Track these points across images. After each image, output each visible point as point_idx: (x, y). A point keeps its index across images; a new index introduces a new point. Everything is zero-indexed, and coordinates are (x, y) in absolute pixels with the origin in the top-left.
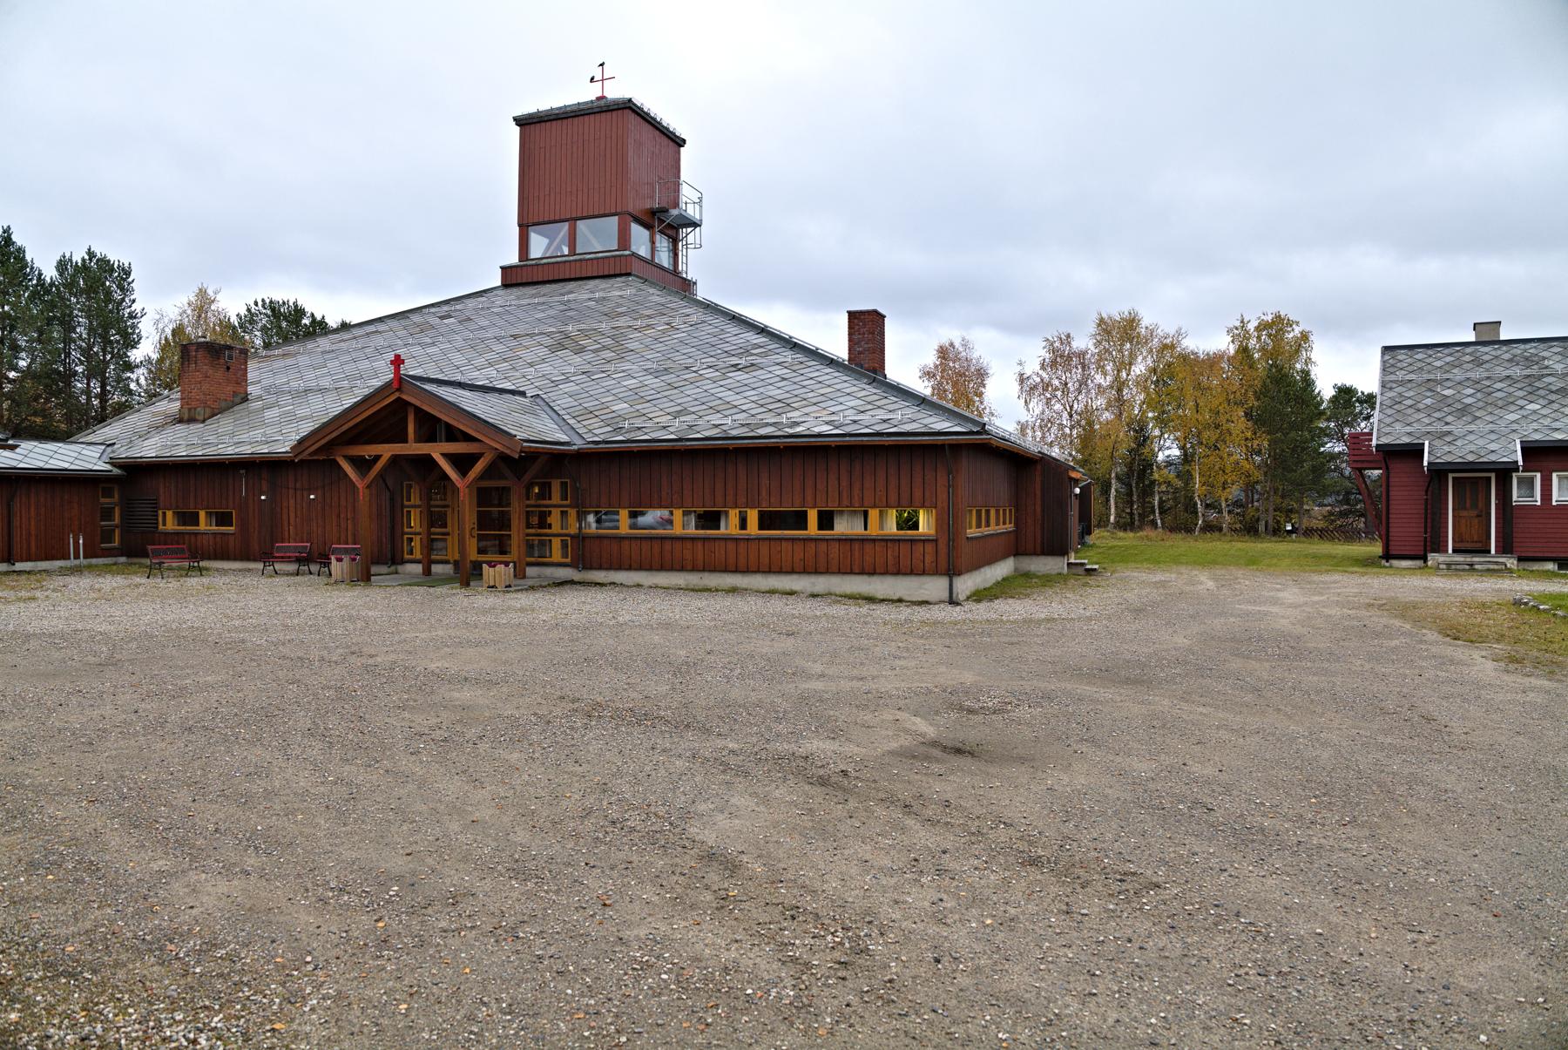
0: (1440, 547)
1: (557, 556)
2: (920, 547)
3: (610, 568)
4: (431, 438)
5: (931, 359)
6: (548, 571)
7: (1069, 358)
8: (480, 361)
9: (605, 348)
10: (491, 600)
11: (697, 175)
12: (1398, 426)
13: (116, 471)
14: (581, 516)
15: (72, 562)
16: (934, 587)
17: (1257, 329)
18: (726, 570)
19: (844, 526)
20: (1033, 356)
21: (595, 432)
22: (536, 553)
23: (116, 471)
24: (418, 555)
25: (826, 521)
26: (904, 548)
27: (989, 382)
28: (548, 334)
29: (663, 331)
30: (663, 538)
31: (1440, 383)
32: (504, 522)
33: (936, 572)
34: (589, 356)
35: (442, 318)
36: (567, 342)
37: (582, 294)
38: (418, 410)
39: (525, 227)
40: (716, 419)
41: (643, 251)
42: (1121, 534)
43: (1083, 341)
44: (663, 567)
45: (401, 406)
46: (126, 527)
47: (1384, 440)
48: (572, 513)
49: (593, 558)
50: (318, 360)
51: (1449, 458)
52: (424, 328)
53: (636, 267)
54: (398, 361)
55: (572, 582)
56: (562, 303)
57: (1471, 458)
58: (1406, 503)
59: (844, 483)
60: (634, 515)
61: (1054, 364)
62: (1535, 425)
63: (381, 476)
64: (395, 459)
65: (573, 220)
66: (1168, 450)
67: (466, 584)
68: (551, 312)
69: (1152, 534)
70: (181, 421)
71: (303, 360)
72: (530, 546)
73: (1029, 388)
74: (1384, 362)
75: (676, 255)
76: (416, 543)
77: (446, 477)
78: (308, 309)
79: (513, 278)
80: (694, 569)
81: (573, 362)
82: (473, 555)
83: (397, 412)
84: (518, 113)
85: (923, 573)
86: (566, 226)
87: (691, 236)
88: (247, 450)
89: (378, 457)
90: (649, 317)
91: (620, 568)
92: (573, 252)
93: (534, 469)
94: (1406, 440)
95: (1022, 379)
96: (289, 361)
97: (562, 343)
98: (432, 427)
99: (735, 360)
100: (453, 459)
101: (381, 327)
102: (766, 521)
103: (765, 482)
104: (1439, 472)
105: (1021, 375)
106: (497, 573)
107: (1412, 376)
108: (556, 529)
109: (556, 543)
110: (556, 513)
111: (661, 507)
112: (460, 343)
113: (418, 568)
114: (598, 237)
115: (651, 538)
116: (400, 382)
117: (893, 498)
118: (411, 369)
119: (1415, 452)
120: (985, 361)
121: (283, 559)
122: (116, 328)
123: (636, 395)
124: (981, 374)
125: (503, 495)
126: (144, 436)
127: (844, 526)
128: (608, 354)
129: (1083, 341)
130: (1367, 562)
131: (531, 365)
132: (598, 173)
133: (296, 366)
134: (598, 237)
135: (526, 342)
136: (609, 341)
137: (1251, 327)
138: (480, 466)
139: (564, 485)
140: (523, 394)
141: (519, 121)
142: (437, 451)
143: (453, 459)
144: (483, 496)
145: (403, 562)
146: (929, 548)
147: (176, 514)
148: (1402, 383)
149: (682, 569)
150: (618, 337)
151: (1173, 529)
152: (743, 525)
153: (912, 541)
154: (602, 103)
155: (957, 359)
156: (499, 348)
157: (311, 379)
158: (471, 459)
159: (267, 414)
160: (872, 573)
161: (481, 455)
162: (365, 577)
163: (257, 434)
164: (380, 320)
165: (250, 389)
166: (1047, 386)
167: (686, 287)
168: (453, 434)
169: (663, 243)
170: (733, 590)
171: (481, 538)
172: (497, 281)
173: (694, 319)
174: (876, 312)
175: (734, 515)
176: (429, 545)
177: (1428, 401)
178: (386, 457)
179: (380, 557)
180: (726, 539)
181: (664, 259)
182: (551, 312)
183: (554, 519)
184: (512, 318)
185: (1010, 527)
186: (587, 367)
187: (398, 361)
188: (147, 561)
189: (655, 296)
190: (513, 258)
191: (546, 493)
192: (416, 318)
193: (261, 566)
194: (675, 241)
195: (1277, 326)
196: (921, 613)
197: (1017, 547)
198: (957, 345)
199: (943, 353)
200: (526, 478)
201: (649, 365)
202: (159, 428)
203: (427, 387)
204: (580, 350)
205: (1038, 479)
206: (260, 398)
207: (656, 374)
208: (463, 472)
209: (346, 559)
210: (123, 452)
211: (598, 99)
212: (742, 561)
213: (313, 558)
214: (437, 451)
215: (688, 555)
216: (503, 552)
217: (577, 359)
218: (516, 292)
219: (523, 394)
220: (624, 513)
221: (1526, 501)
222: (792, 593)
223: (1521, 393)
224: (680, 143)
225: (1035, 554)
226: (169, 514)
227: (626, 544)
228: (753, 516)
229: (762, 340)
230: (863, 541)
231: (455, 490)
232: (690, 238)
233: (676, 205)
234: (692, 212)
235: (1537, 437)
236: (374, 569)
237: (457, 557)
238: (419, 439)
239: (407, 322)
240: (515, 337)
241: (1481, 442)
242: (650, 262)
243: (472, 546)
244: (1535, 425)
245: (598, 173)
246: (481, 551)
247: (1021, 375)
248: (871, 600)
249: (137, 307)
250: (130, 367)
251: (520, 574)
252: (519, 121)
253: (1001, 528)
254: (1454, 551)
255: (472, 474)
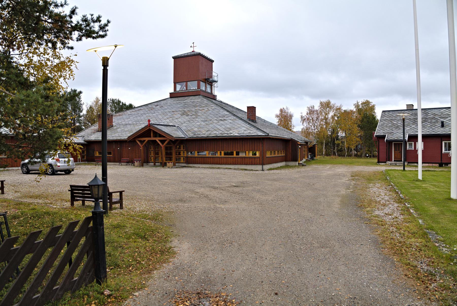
0: (390, 159)
1: (182, 161)
2: (256, 159)
3: (193, 163)
4: (156, 137)
5: (278, 113)
6: (180, 164)
7: (314, 112)
8: (165, 118)
9: (193, 115)
10: (169, 169)
11: (217, 70)
12: (381, 131)
13: (86, 143)
14: (187, 152)
15: (78, 163)
16: (259, 167)
17: (361, 104)
18: (217, 164)
19: (241, 155)
20: (305, 112)
21: (190, 135)
22: (178, 160)
23: (86, 143)
24: (152, 161)
25: (238, 154)
26: (253, 159)
27: (293, 118)
28: (181, 111)
29: (206, 111)
30: (204, 157)
31: (394, 120)
32: (171, 154)
33: (259, 164)
34: (190, 117)
35: (156, 106)
36: (185, 113)
37: (189, 100)
38: (153, 131)
39: (175, 83)
40: (215, 132)
41: (203, 88)
42: (326, 157)
43: (317, 107)
44: (204, 163)
45: (150, 130)
46: (87, 155)
47: (377, 134)
48: (185, 152)
49: (190, 161)
50: (128, 117)
51: (391, 139)
52: (152, 109)
53: (202, 93)
54: (149, 121)
55: (185, 167)
56: (184, 103)
57: (396, 139)
58: (383, 148)
59: (241, 146)
60: (198, 152)
61: (310, 113)
62: (413, 131)
63: (145, 145)
64: (148, 141)
65: (187, 82)
66: (341, 134)
67: (163, 167)
68: (182, 105)
69: (334, 157)
70: (98, 131)
71: (124, 116)
72: (177, 160)
73: (303, 119)
74: (382, 115)
75: (212, 89)
76: (152, 158)
77: (159, 144)
78: (122, 101)
79: (172, 96)
80: (211, 164)
81: (186, 118)
82: (165, 161)
83: (149, 131)
84: (173, 56)
85: (257, 164)
86: (185, 83)
87: (215, 84)
88: (115, 138)
89: (145, 141)
90: (204, 107)
91: (195, 163)
92: (187, 89)
93: (178, 142)
94: (382, 134)
95: (302, 117)
96: (121, 117)
97: (184, 113)
98: (157, 134)
99: (221, 118)
100: (160, 141)
101: (142, 108)
102: (225, 154)
103: (256, 145)
104: (390, 142)
105: (302, 116)
106: (170, 164)
107: (388, 118)
108: (182, 155)
109: (182, 158)
110: (182, 152)
111: (206, 151)
112: (160, 113)
113: (153, 164)
114: (193, 86)
115: (202, 157)
116: (150, 125)
117: (251, 149)
118: (152, 122)
119: (384, 137)
120: (292, 113)
121: (124, 162)
122: (77, 107)
123: (199, 127)
124: (291, 116)
125: (171, 148)
126: (91, 135)
127: (241, 155)
128: (194, 116)
129: (317, 107)
130: (373, 164)
131: (177, 119)
132: (193, 71)
133: (123, 118)
134: (193, 86)
135: (176, 113)
136: (194, 113)
137: (360, 103)
138: (166, 142)
139: (184, 146)
140: (175, 126)
141: (173, 58)
142: (157, 139)
143: (160, 141)
144: (166, 148)
145: (149, 162)
146: (258, 159)
147: (99, 152)
148: (385, 120)
149: (208, 164)
150: (196, 112)
151: (339, 155)
152: (221, 155)
153: (255, 158)
154: (193, 53)
155: (285, 112)
156: (169, 114)
157: (127, 121)
158: (165, 141)
159: (118, 130)
160: (247, 164)
161: (166, 140)
162: (142, 166)
163: (117, 135)
164: (141, 106)
165: (113, 124)
166: (308, 119)
167: (213, 98)
168: (160, 136)
169: (208, 87)
170: (219, 168)
171: (166, 157)
172: (168, 96)
173: (213, 108)
174: (253, 107)
175: (219, 152)
176: (155, 158)
177: (390, 125)
178: (147, 140)
179: (145, 162)
180: (217, 157)
181: (209, 90)
182: (182, 105)
183: (182, 153)
184: (172, 107)
185: (284, 155)
186: (188, 120)
187: (149, 121)
188: (95, 163)
189: (205, 101)
190: (172, 91)
191: (180, 148)
192: (150, 106)
193: (118, 163)
194: (211, 86)
195: (367, 103)
196: (257, 172)
197: (285, 159)
198: (285, 108)
199: (281, 111)
200: (176, 144)
201: (202, 119)
202: (94, 133)
203: (155, 126)
204: (188, 115)
205: (290, 146)
206: (116, 126)
207: (204, 121)
208: (163, 143)
209: (138, 162)
210: (87, 139)
211: (193, 51)
212: (220, 162)
213: (130, 162)
214: (157, 139)
215: (209, 161)
216: (171, 160)
217: (187, 118)
218: (173, 99)
219: (175, 126)
220: (196, 152)
221: (410, 149)
222: (230, 169)
223: (412, 123)
224: (212, 61)
225: (290, 161)
226: (97, 152)
227: (196, 159)
228: (223, 152)
229: (228, 113)
230: (245, 158)
231: (140, 147)
232: (215, 85)
233: (211, 77)
234: (215, 79)
235: (412, 133)
236: (144, 164)
237: (161, 161)
238: (153, 137)
239: (147, 107)
240: (173, 111)
241: (399, 135)
242: (205, 92)
243: (164, 159)
244: (413, 131)
245: (193, 71)
246: (166, 160)
247: (302, 116)
248: (246, 170)
249: (82, 102)
250: (81, 117)
251: (174, 165)
252: (173, 58)
253: (283, 155)
254: (394, 161)
255: (165, 144)
